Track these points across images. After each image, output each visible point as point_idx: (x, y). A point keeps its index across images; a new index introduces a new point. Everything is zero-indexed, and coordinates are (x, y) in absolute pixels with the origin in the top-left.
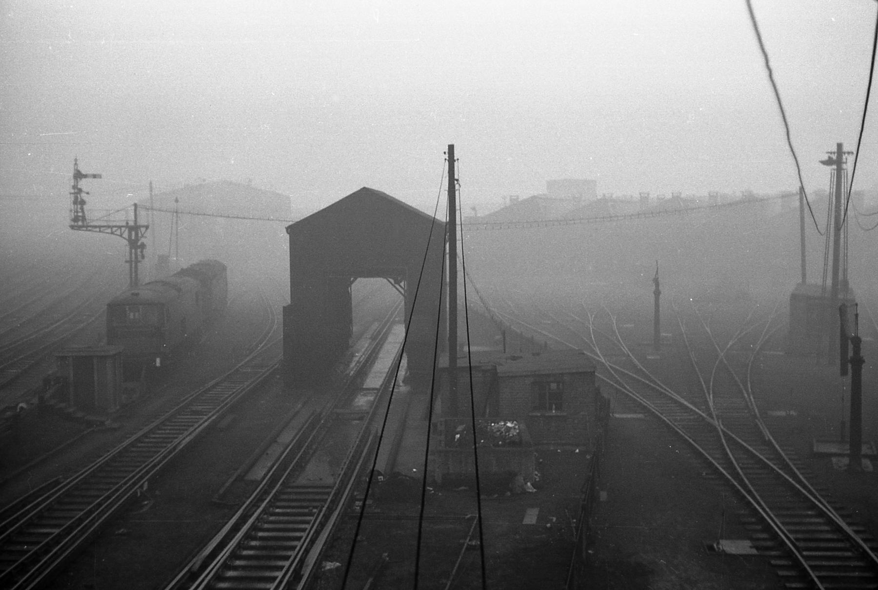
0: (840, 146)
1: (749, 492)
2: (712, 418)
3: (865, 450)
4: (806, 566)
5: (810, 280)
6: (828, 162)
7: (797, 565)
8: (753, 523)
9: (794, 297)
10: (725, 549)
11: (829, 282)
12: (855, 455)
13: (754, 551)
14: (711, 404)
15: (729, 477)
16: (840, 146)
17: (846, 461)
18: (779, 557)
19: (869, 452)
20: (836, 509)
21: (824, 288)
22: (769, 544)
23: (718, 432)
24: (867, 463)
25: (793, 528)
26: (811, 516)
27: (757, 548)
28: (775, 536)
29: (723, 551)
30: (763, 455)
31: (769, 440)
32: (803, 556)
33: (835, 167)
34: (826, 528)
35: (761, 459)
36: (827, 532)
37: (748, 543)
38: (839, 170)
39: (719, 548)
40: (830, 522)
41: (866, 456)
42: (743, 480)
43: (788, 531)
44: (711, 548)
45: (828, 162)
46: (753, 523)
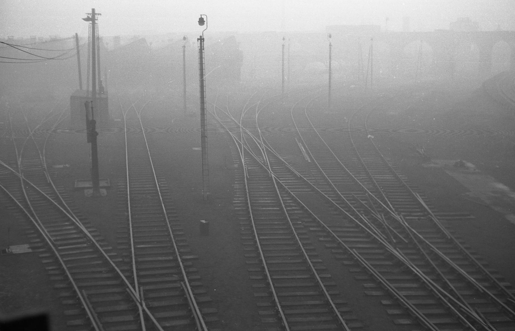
0: (93, 10)
1: (33, 215)
2: (18, 172)
3: (102, 184)
4: (58, 255)
5: (85, 88)
6: (87, 19)
7: (53, 255)
8: (32, 233)
9: (73, 98)
10: (13, 251)
11: (91, 89)
12: (96, 186)
13: (30, 250)
14: (19, 163)
15: (22, 207)
16: (93, 10)
17: (91, 191)
18: (287, 197)
19: (106, 185)
20: (80, 220)
21: (88, 91)
22: (40, 245)
23: (20, 181)
24: (104, 192)
25: (54, 234)
26: (67, 225)
27: (32, 248)
28: (44, 240)
29: (12, 252)
30: (44, 192)
31: (50, 183)
32: (59, 251)
33: (91, 22)
34: (74, 231)
35: (43, 195)
36: (75, 233)
37: (26, 246)
38: (94, 24)
39: (9, 251)
40: (77, 228)
41: (102, 187)
42: (30, 208)
43: (51, 236)
44: (4, 251)
45: (87, 19)
46: (32, 233)
